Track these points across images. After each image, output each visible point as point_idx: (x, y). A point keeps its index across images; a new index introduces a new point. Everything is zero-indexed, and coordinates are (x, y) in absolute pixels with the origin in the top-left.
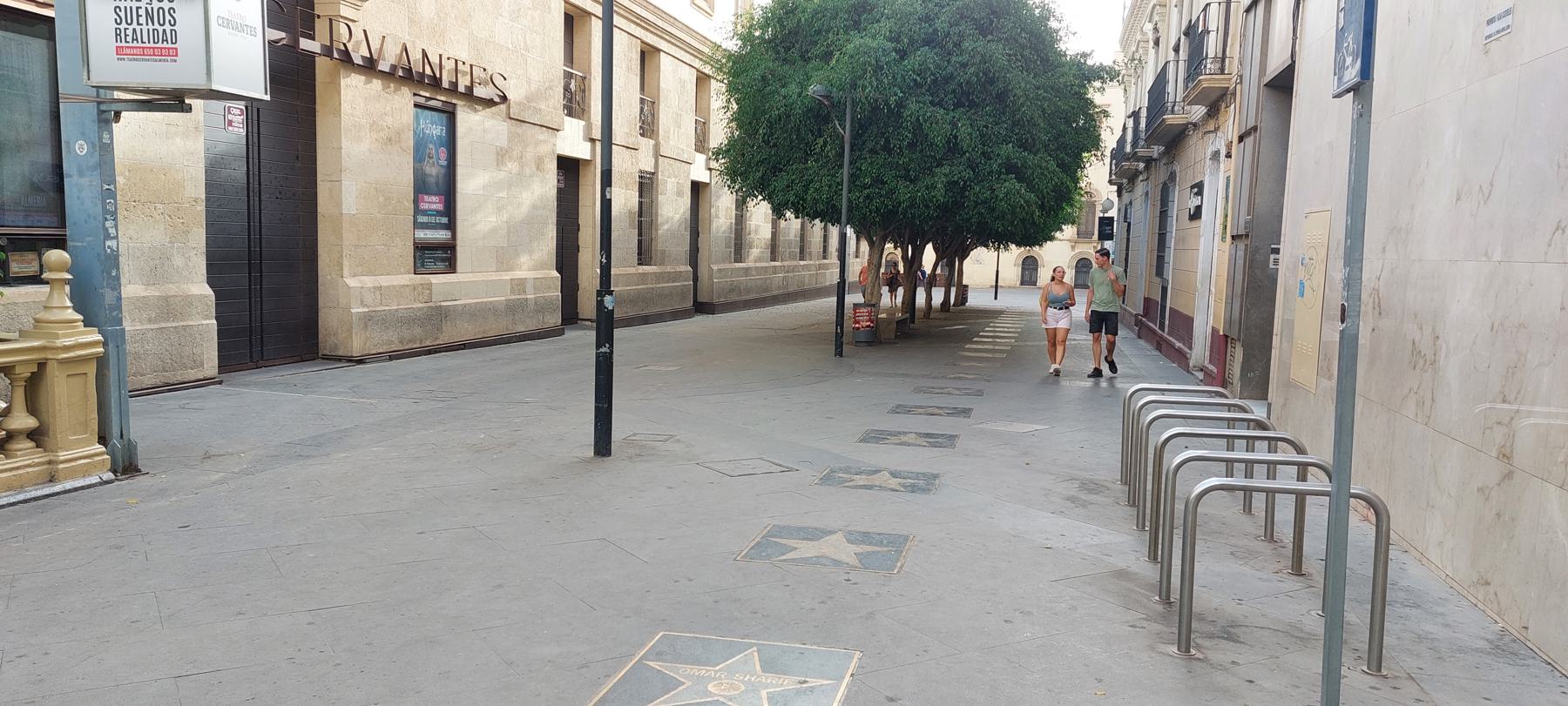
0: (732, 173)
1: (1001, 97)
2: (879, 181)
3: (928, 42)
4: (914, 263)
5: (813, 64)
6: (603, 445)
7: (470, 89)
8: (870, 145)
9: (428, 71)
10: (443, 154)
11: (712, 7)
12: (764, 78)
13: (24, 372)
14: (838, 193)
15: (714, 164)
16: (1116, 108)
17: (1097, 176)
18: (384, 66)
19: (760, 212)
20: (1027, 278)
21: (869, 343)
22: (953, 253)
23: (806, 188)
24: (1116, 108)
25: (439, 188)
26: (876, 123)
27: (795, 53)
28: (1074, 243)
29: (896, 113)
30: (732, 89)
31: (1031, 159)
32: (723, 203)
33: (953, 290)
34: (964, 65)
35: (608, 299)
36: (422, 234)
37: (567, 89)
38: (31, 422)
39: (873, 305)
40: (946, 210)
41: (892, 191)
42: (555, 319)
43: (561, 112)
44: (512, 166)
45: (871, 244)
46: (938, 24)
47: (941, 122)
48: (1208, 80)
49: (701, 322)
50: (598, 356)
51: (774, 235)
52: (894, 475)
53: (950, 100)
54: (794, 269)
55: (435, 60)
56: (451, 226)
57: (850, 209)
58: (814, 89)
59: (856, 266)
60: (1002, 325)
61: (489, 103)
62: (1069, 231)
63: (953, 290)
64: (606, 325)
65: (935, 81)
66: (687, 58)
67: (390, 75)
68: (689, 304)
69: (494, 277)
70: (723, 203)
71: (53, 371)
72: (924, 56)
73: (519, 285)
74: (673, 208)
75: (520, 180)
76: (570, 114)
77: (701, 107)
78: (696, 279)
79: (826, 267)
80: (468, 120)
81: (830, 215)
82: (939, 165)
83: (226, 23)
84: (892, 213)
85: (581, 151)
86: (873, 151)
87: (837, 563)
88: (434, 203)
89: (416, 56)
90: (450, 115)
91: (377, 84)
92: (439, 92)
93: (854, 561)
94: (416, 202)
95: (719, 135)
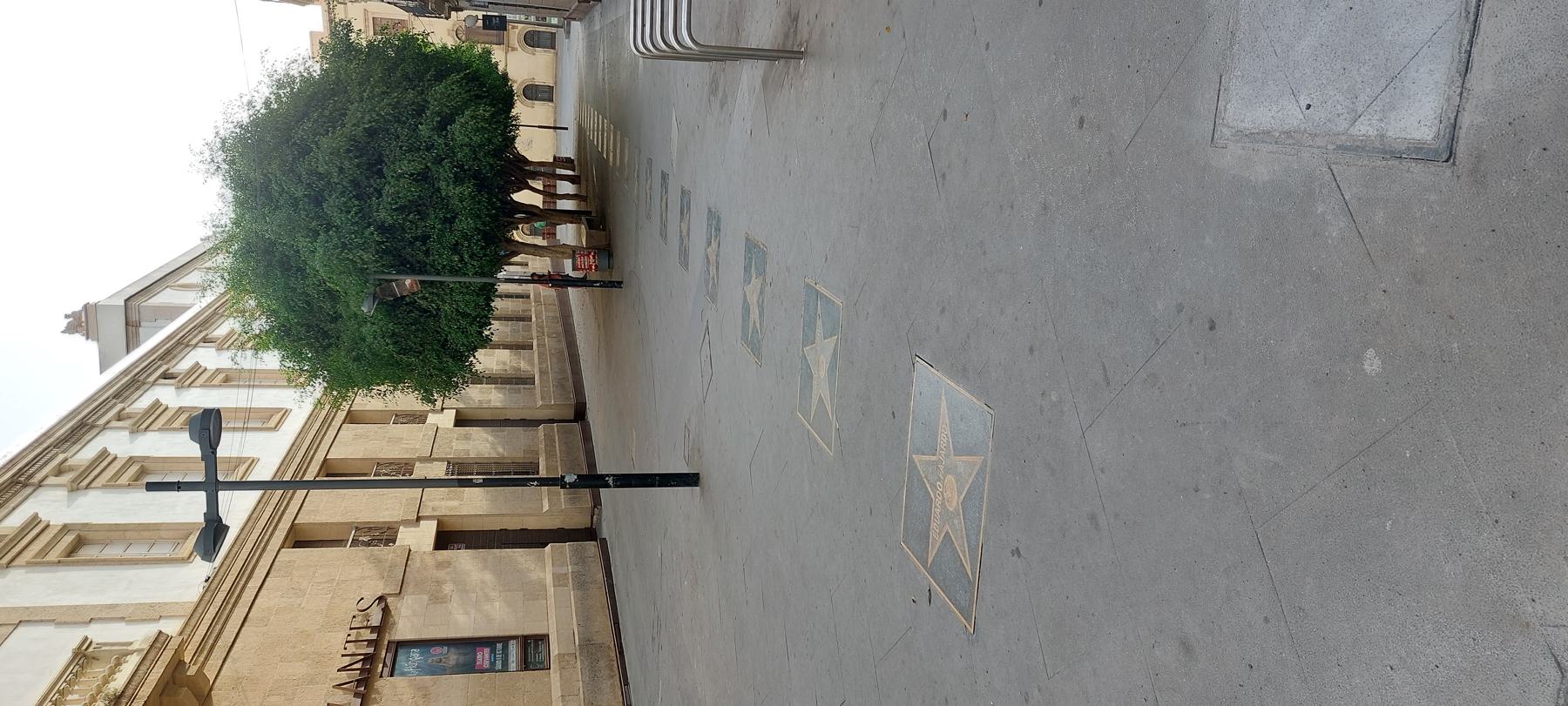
0: (449, 386)
1: (371, 133)
2: (455, 248)
3: (318, 201)
4: (531, 213)
5: (340, 308)
6: (690, 480)
7: (373, 629)
8: (421, 256)
9: (359, 666)
10: (438, 650)
11: (278, 410)
12: (357, 359)
14: (467, 286)
15: (439, 404)
17: (440, 32)
19: (486, 360)
20: (546, 95)
21: (610, 255)
22: (521, 171)
23: (465, 315)
28: (509, 48)
30: (368, 384)
32: (477, 396)
33: (560, 171)
34: (341, 170)
35: (567, 479)
36: (513, 666)
37: (368, 544)
39: (573, 252)
40: (481, 183)
41: (465, 237)
42: (591, 547)
43: (392, 548)
45: (515, 254)
46: (299, 194)
47: (396, 188)
49: (592, 415)
50: (616, 486)
51: (506, 347)
52: (709, 244)
53: (375, 182)
54: (540, 326)
55: (347, 661)
56: (505, 640)
57: (483, 275)
58: (366, 309)
59: (541, 265)
60: (593, 136)
61: (386, 611)
62: (498, 55)
63: (560, 171)
64: (592, 481)
65: (357, 197)
66: (332, 433)
68: (577, 426)
69: (551, 601)
70: (477, 396)
73: (559, 580)
74: (481, 444)
75: (462, 587)
76: (394, 541)
77: (379, 418)
78: (552, 421)
79: (538, 295)
80: (403, 629)
81: (488, 292)
82: (439, 190)
84: (485, 235)
85: (429, 530)
86: (427, 253)
87: (762, 292)
88: (483, 657)
93: (760, 281)
94: (482, 671)
95: (407, 400)
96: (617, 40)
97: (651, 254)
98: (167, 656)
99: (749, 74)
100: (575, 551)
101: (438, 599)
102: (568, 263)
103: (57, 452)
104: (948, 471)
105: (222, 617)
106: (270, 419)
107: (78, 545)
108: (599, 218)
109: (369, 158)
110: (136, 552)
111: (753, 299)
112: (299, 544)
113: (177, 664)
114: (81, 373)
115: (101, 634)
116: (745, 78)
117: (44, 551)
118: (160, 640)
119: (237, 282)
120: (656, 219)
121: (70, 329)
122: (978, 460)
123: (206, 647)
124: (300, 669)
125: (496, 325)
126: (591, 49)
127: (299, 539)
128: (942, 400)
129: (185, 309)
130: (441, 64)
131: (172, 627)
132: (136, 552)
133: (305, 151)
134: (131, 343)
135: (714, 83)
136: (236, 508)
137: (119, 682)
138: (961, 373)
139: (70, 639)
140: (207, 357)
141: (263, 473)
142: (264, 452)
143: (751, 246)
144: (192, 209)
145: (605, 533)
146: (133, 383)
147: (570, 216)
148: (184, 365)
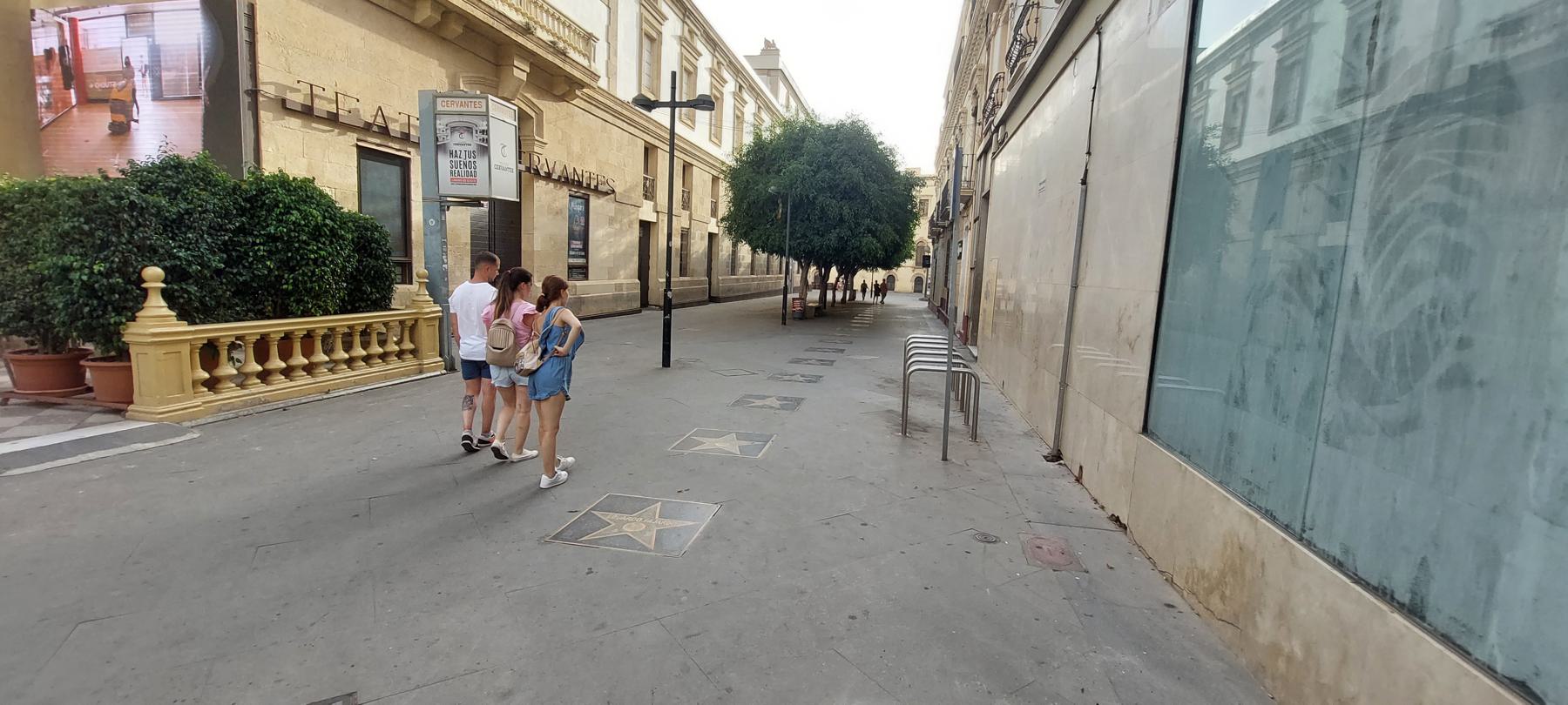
0: (729, 230)
2: (804, 236)
3: (829, 167)
6: (666, 362)
10: (583, 220)
13: (409, 324)
16: (929, 196)
17: (921, 232)
18: (555, 177)
19: (745, 250)
22: (848, 272)
24: (929, 196)
25: (580, 236)
26: (802, 206)
27: (763, 169)
29: (812, 203)
30: (733, 186)
31: (880, 227)
32: (725, 244)
38: (412, 346)
39: (803, 299)
42: (637, 305)
44: (617, 226)
47: (833, 206)
48: (964, 192)
49: (712, 305)
53: (839, 196)
56: (586, 257)
59: (797, 279)
60: (868, 311)
62: (910, 263)
64: (668, 307)
67: (558, 181)
70: (725, 244)
71: (421, 322)
72: (826, 174)
74: (699, 246)
77: (714, 194)
80: (595, 202)
81: (781, 253)
83: (499, 167)
85: (652, 218)
88: (578, 245)
89: (570, 171)
90: (587, 201)
91: (551, 185)
92: (581, 189)
95: (723, 210)
96: (917, 326)
97: (799, 341)
98: (587, 80)
99: (895, 402)
100: (635, 295)
101: (611, 221)
102: (797, 295)
103: (697, 27)
104: (648, 526)
105: (606, 109)
106: (716, 136)
107: (651, 39)
108: (822, 314)
109: (850, 193)
110: (645, 66)
111: (768, 402)
112: (646, 149)
113: (582, 85)
114: (744, 46)
115: (601, 48)
116: (890, 399)
117: (648, 22)
118: (596, 77)
119: (787, 124)
120: (820, 345)
121: (767, 42)
122: (652, 546)
123: (590, 100)
124: (576, 148)
125: (765, 255)
126: (914, 312)
127: (649, 150)
128: (699, 517)
129: (776, 96)
130: (905, 232)
131: (603, 83)
132: (645, 66)
133: (854, 162)
134: (759, 71)
135: (892, 381)
136: (661, 116)
137: (572, 54)
138: (707, 536)
139: (599, 31)
140: (750, 108)
141: (680, 129)
142: (695, 131)
143: (799, 401)
144: (829, 110)
145: (644, 312)
146: (737, 71)
147: (823, 295)
148: (746, 96)
